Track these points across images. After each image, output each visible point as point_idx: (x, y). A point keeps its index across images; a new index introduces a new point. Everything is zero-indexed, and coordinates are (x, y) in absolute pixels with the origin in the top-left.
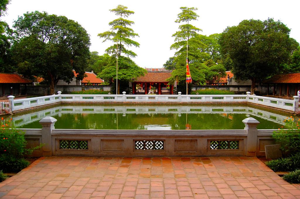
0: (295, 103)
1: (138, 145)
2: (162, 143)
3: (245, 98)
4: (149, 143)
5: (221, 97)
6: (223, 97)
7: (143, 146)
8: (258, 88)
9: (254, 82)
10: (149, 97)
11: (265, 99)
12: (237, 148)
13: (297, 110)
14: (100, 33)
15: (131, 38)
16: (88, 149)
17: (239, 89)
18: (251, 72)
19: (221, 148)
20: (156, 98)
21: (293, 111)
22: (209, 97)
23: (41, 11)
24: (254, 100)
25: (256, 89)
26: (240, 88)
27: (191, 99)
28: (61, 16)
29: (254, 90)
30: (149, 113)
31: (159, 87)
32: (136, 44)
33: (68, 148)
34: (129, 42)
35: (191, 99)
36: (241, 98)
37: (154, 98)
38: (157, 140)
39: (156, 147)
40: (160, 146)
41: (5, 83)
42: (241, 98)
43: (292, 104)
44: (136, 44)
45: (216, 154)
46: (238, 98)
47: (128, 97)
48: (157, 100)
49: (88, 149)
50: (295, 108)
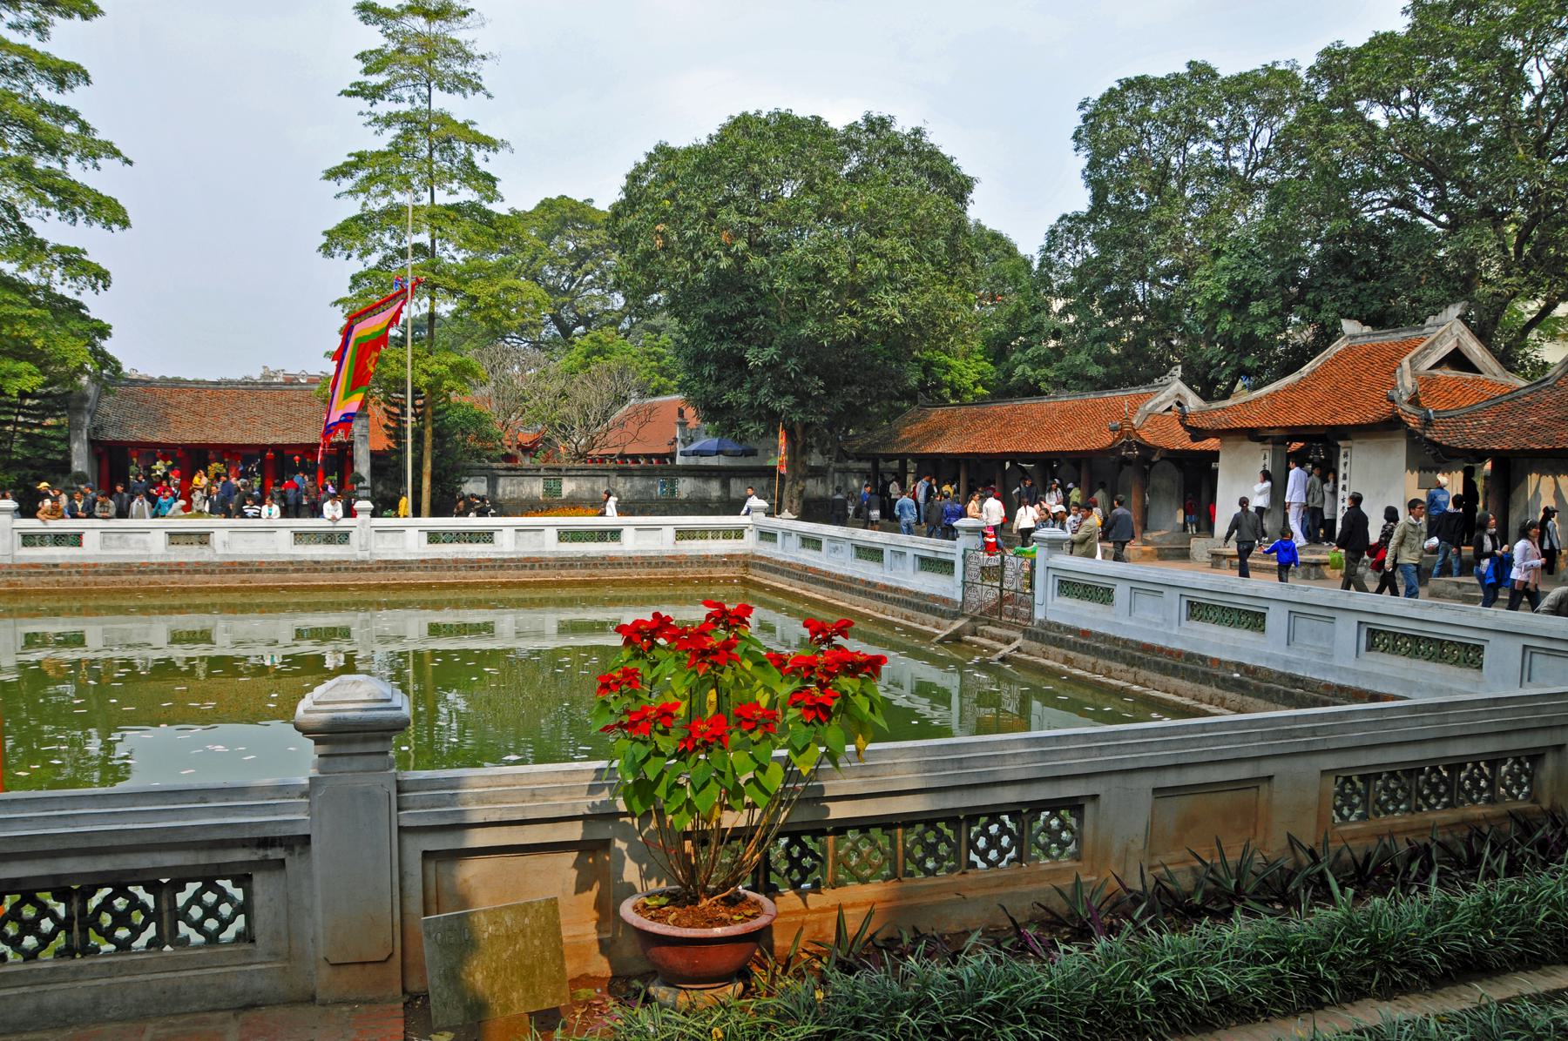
0: (964, 557)
1: (994, 829)
2: (238, 894)
3: (739, 533)
4: (202, 891)
5: (606, 532)
6: (619, 532)
7: (61, 935)
8: (824, 482)
9: (799, 447)
10: (170, 534)
11: (832, 539)
12: (240, 937)
13: (973, 597)
14: (329, 166)
15: (76, 171)
16: (253, 941)
17: (725, 486)
18: (780, 394)
19: (1419, 809)
20: (218, 537)
21: (955, 602)
22: (539, 530)
23: (725, 121)
24: (783, 546)
25: (815, 488)
26: (732, 482)
27: (430, 542)
28: (954, 163)
29: (801, 492)
30: (179, 653)
31: (289, 472)
32: (110, 213)
33: (67, 952)
34: (70, 198)
35: (430, 542)
36: (717, 533)
37: (203, 538)
38: (135, 872)
39: (183, 929)
40: (113, 928)
41: (1086, 451)
42: (717, 533)
43: (952, 563)
44: (110, 213)
45: (30, 1004)
46: (702, 534)
47: (33, 536)
48: (220, 550)
49: (253, 941)
50: (964, 583)
